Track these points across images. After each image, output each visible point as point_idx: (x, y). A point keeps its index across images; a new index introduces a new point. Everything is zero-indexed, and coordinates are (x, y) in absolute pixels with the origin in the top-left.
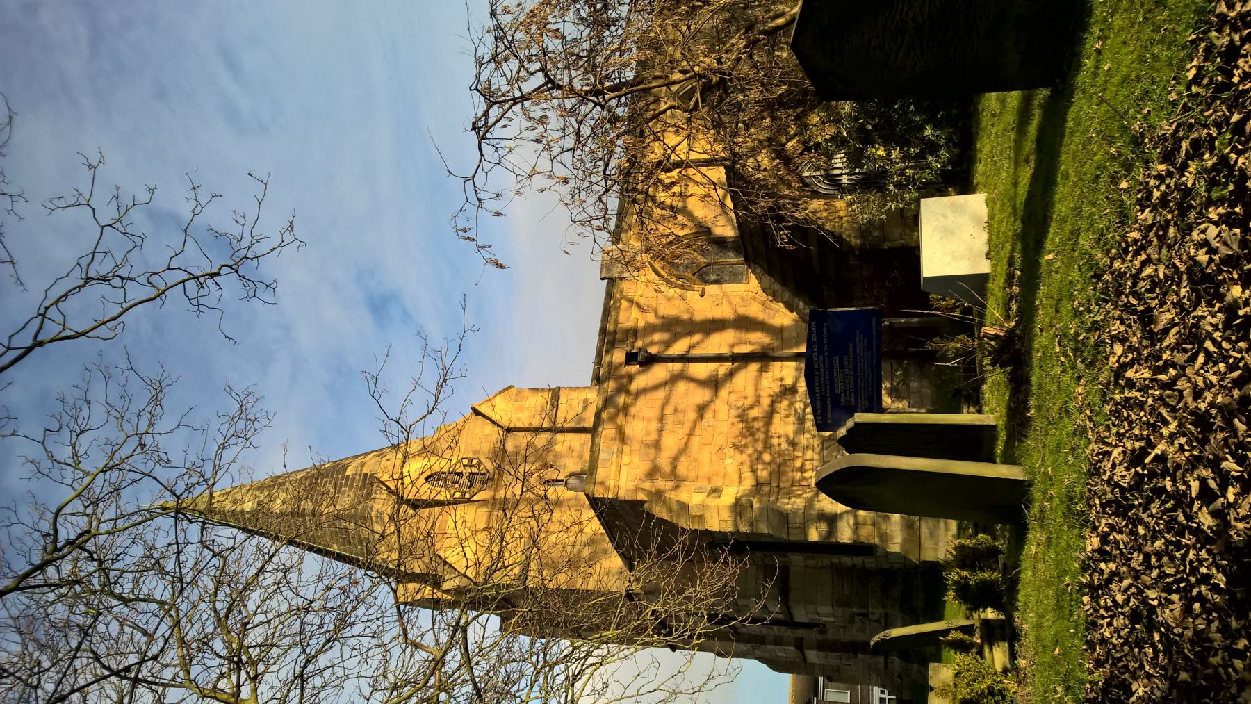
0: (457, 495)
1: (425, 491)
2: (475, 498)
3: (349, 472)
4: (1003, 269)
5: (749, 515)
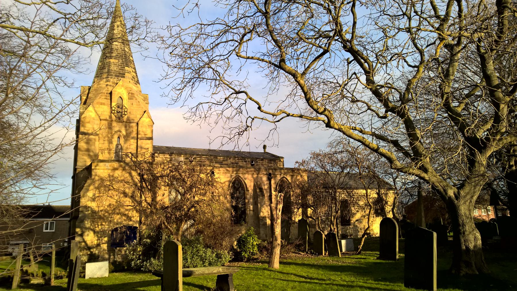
0: (113, 109)
1: (115, 98)
2: (112, 114)
3: (126, 68)
4: (86, 282)
5: (85, 210)
